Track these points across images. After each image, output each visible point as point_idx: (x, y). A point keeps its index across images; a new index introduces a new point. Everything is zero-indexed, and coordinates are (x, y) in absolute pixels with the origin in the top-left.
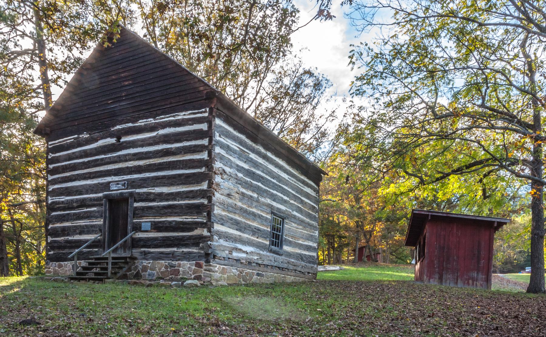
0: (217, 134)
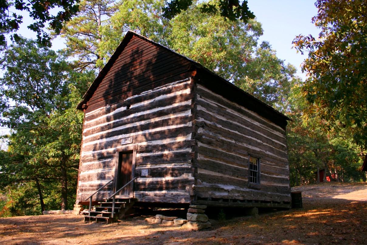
0: (199, 96)
